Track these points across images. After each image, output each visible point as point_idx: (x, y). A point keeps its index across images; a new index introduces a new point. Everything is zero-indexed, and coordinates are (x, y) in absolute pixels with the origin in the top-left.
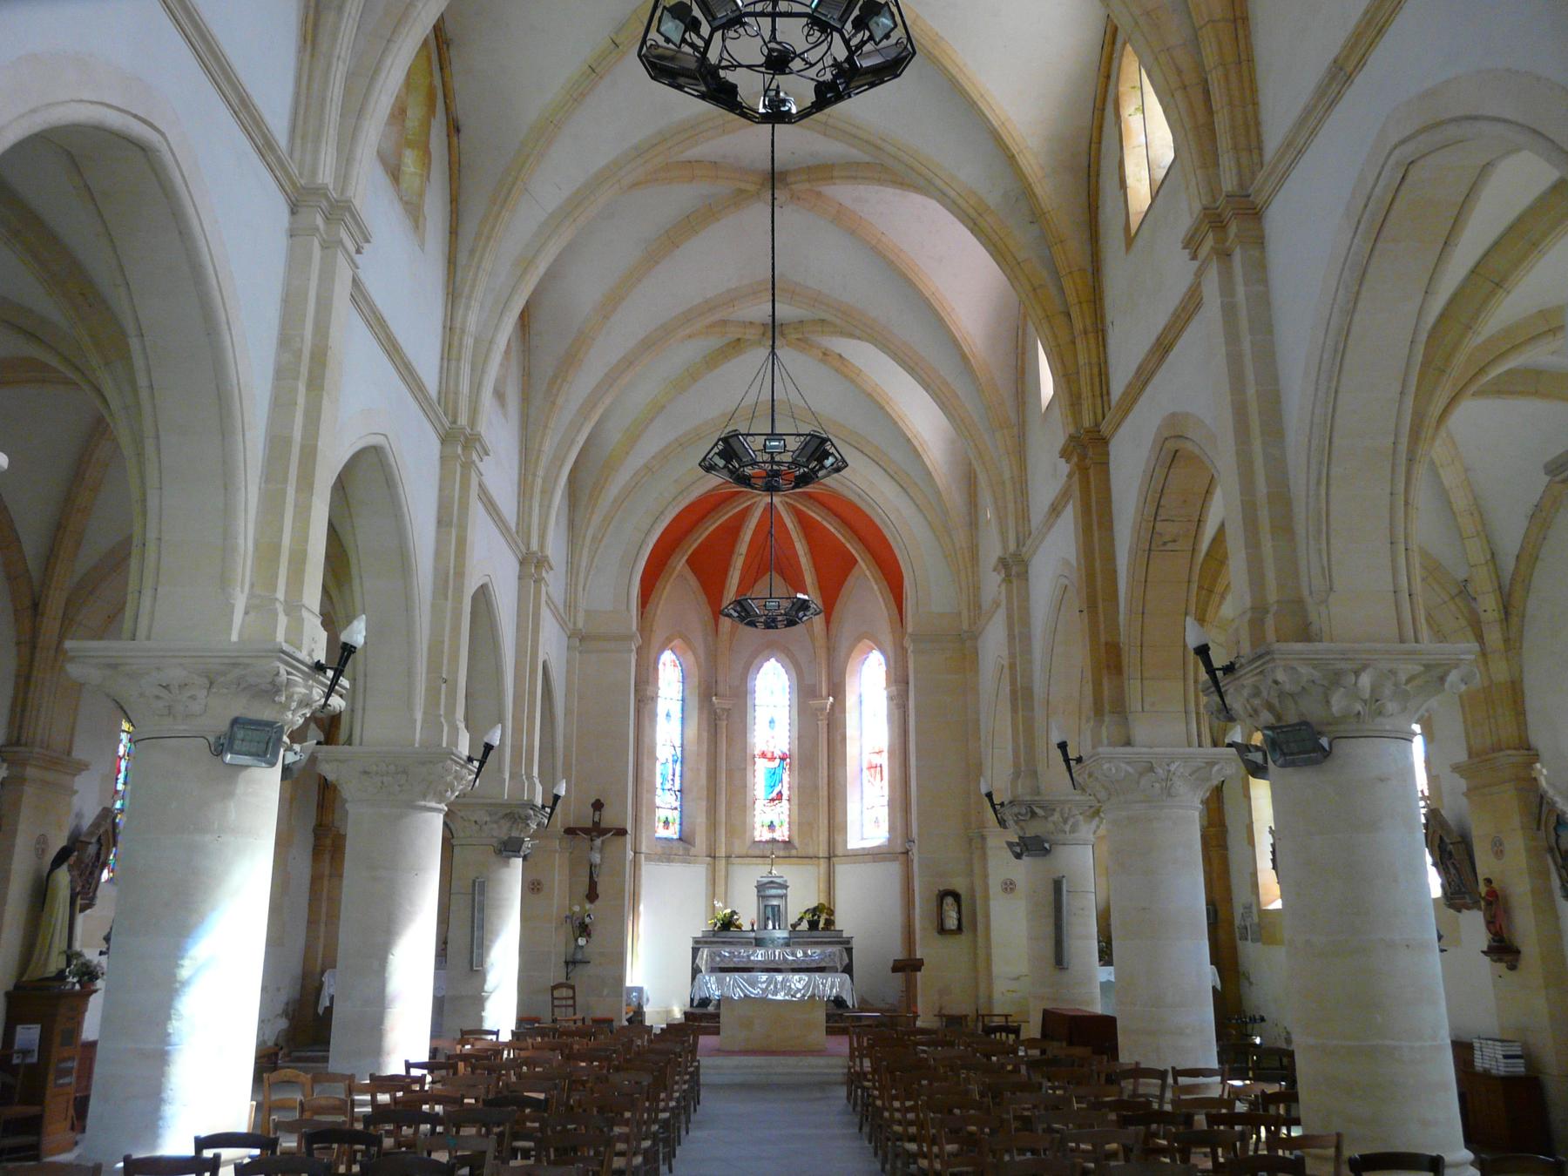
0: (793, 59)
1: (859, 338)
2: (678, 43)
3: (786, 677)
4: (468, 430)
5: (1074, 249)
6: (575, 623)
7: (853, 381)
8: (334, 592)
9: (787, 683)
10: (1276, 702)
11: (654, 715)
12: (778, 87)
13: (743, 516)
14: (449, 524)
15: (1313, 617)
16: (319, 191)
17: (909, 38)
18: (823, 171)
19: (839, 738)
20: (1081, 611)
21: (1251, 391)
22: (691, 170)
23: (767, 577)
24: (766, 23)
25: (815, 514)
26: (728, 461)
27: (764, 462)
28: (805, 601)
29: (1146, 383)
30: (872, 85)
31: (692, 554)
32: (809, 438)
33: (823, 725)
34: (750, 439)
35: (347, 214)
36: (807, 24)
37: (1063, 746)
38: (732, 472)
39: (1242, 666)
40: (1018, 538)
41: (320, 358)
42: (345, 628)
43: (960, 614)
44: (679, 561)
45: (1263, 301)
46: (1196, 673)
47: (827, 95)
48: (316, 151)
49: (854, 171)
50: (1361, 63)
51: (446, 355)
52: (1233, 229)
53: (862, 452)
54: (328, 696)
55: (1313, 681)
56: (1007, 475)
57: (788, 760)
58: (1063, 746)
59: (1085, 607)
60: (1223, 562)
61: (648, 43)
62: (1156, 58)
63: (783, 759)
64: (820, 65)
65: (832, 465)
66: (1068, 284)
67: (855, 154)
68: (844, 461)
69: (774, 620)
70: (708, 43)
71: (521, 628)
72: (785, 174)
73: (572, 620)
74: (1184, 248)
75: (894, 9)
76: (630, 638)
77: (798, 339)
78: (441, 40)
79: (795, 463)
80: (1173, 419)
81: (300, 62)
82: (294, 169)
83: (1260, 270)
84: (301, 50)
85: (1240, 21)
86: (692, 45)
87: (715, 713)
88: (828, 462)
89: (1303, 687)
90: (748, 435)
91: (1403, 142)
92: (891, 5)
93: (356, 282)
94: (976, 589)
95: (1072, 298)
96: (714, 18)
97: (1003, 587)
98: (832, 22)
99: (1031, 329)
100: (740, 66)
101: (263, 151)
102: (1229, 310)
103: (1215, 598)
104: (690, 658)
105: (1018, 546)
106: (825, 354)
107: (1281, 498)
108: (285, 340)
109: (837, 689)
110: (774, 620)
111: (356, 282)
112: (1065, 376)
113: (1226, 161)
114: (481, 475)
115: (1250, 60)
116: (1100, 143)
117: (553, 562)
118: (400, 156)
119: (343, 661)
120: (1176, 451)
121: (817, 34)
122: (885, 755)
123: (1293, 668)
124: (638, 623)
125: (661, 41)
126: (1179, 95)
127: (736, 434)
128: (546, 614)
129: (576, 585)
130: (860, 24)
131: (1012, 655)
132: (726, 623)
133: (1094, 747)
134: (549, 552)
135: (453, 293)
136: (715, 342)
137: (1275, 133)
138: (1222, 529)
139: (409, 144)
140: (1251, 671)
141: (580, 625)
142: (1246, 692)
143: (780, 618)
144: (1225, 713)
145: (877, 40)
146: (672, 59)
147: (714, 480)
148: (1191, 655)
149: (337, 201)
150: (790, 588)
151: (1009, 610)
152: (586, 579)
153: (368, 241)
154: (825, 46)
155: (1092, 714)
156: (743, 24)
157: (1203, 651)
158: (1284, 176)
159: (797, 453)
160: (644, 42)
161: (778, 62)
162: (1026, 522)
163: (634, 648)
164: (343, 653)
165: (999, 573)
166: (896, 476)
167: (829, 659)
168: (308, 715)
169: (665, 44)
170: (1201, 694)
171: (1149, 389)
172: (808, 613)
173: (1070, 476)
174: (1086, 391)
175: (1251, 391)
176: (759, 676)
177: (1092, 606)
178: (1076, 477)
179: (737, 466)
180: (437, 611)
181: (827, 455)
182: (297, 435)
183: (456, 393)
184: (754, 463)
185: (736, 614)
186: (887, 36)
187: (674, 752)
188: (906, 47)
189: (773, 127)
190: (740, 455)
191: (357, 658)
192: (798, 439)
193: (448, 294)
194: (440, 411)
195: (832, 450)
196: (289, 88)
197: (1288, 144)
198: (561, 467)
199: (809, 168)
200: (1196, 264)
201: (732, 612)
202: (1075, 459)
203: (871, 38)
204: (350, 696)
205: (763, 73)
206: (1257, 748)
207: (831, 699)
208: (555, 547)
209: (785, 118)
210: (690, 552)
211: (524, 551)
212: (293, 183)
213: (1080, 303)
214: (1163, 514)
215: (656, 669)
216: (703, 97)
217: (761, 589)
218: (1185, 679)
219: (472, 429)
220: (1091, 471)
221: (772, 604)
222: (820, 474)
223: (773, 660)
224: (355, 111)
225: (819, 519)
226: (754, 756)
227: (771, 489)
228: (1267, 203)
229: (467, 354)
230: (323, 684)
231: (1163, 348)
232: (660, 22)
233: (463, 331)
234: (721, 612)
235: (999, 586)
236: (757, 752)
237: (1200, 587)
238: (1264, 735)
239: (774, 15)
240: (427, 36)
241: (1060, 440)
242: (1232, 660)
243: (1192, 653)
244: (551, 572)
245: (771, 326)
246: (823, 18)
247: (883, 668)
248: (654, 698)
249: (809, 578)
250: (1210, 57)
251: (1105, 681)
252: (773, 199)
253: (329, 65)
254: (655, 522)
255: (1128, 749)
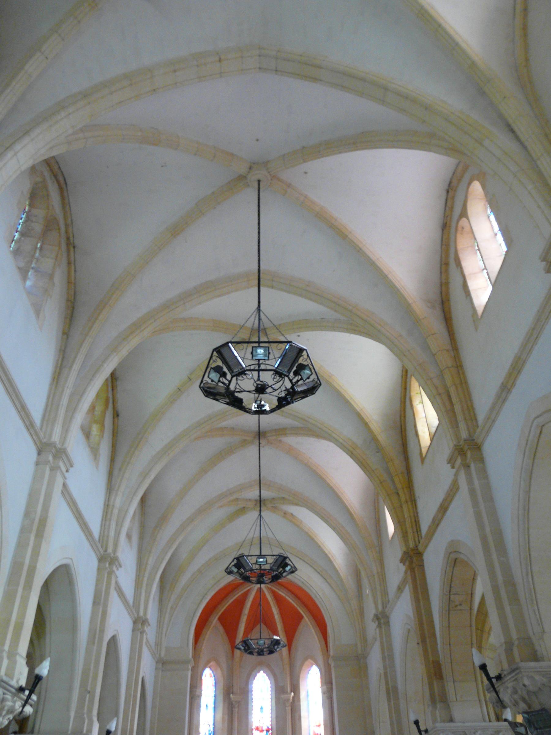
0: (268, 388)
1: (301, 506)
2: (217, 382)
3: (269, 681)
4: (112, 555)
5: (398, 463)
6: (160, 654)
7: (298, 526)
8: (35, 642)
9: (270, 685)
10: (526, 697)
11: (199, 706)
12: (261, 399)
13: (245, 595)
14: (99, 604)
15: (537, 647)
16: (51, 445)
17: (318, 379)
18: (282, 431)
19: (297, 717)
20: (418, 644)
21: (488, 530)
22: (223, 431)
23: (258, 626)
24: (255, 374)
25: (282, 593)
26: (239, 569)
27: (256, 569)
28: (278, 640)
29: (438, 525)
30: (303, 398)
31: (221, 614)
32: (278, 557)
33: (289, 709)
34: (249, 558)
35: (64, 455)
36: (274, 374)
37: (417, 723)
38: (241, 575)
39: (505, 676)
40: (383, 604)
41: (43, 523)
42: (38, 665)
43: (357, 644)
44: (215, 618)
45: (487, 487)
46: (482, 682)
47: (282, 403)
48: (53, 426)
49: (297, 431)
50: (513, 384)
51: (104, 518)
52: (469, 454)
53: (304, 561)
54: (24, 706)
55: (544, 684)
56: (375, 572)
57: (270, 732)
58: (417, 723)
59: (420, 641)
60: (486, 615)
61: (204, 382)
62: (426, 383)
63: (268, 731)
64: (279, 390)
65: (290, 570)
66: (396, 480)
67: (296, 423)
68: (295, 567)
69: (262, 651)
70: (230, 382)
71: (131, 659)
72: (265, 433)
73: (159, 653)
74: (448, 463)
75: (311, 367)
76: (188, 662)
77: (272, 507)
78: (113, 377)
79: (271, 569)
80: (452, 543)
81: (50, 389)
82: (42, 435)
83: (483, 472)
84: (51, 385)
85: (459, 368)
86: (223, 383)
87: (232, 704)
88: (288, 568)
89: (540, 689)
90: (248, 556)
91: (538, 417)
92: (310, 365)
93: (65, 485)
94: (363, 631)
95: (399, 486)
96: (233, 372)
97: (378, 630)
98: (284, 373)
99: (381, 500)
100: (244, 391)
101: (29, 428)
102: (472, 491)
103: (485, 636)
104: (219, 672)
105: (383, 608)
106: (285, 513)
107: (510, 583)
108: (27, 514)
109: (296, 689)
110: (262, 651)
111: (65, 485)
112: (399, 522)
113: (462, 425)
114: (117, 577)
115: (466, 383)
116: (405, 417)
117: (150, 621)
118: (90, 428)
119: (35, 685)
120: (456, 559)
121: (278, 378)
122: (322, 727)
123: (532, 677)
124: (192, 653)
125: (209, 381)
126: (437, 397)
127: (242, 556)
128: (145, 650)
129: (162, 633)
130: (296, 373)
131: (385, 668)
132: (237, 653)
133: (433, 723)
134: (149, 616)
135: (110, 488)
136: (233, 509)
137: (482, 413)
138: (483, 598)
139: (95, 422)
140: (511, 678)
141: (163, 655)
142: (510, 691)
143: (265, 650)
144: (500, 703)
145: (304, 379)
146: (214, 388)
147: (231, 578)
148: (478, 669)
149: (60, 449)
150: (270, 632)
151: (382, 643)
152: (167, 630)
153: (72, 466)
154: (281, 382)
155: (430, 703)
156: (245, 374)
157: (483, 667)
158: (488, 432)
159: (273, 564)
160: (202, 381)
161: (261, 389)
162: (386, 595)
163: (190, 667)
164: (35, 680)
165: (375, 623)
166: (320, 573)
167: (290, 669)
168: (11, 718)
169: (211, 382)
170: (486, 692)
171: (439, 528)
172: (280, 647)
173: (406, 572)
174: (410, 531)
175: (488, 530)
176: (255, 682)
177: (423, 640)
178: (409, 572)
179: (243, 571)
180: (88, 651)
181: (287, 565)
182: (27, 561)
183: (108, 536)
184: (251, 570)
185: (242, 648)
186: (308, 378)
187: (209, 729)
188: (317, 382)
189: (259, 416)
190: (245, 566)
191: (42, 685)
192: (273, 557)
193: (107, 489)
194: (99, 545)
195: (290, 563)
196: (44, 400)
197: (488, 418)
198: (157, 572)
199: (275, 430)
200: (454, 471)
201: (241, 647)
202: (407, 563)
203: (302, 379)
204: (36, 707)
205: (254, 393)
206: (521, 725)
207: (292, 694)
208: (152, 614)
209: (264, 412)
210: (220, 614)
211: (136, 615)
212: (41, 441)
213: (403, 488)
214: (453, 591)
215: (201, 679)
216: (228, 404)
217: (255, 634)
218: (476, 681)
219: (114, 554)
220: (416, 570)
221: (261, 642)
222: (284, 574)
223: (262, 672)
224: (72, 409)
225: (284, 595)
226: (252, 730)
227: (260, 582)
228: (483, 443)
229: (114, 518)
230: (21, 699)
231: (443, 509)
232: (209, 373)
233: (113, 506)
234: (236, 647)
235: (375, 630)
236: (254, 727)
237: (477, 629)
238: (523, 717)
239: (259, 371)
240: (108, 377)
241: (399, 554)
242: (500, 672)
243: (478, 668)
244: (149, 627)
245: (259, 501)
246: (281, 371)
247: (319, 675)
248: (200, 696)
249: (280, 626)
250: (449, 382)
251: (435, 682)
252: (260, 443)
253: (63, 391)
254: (202, 599)
255: (452, 724)
